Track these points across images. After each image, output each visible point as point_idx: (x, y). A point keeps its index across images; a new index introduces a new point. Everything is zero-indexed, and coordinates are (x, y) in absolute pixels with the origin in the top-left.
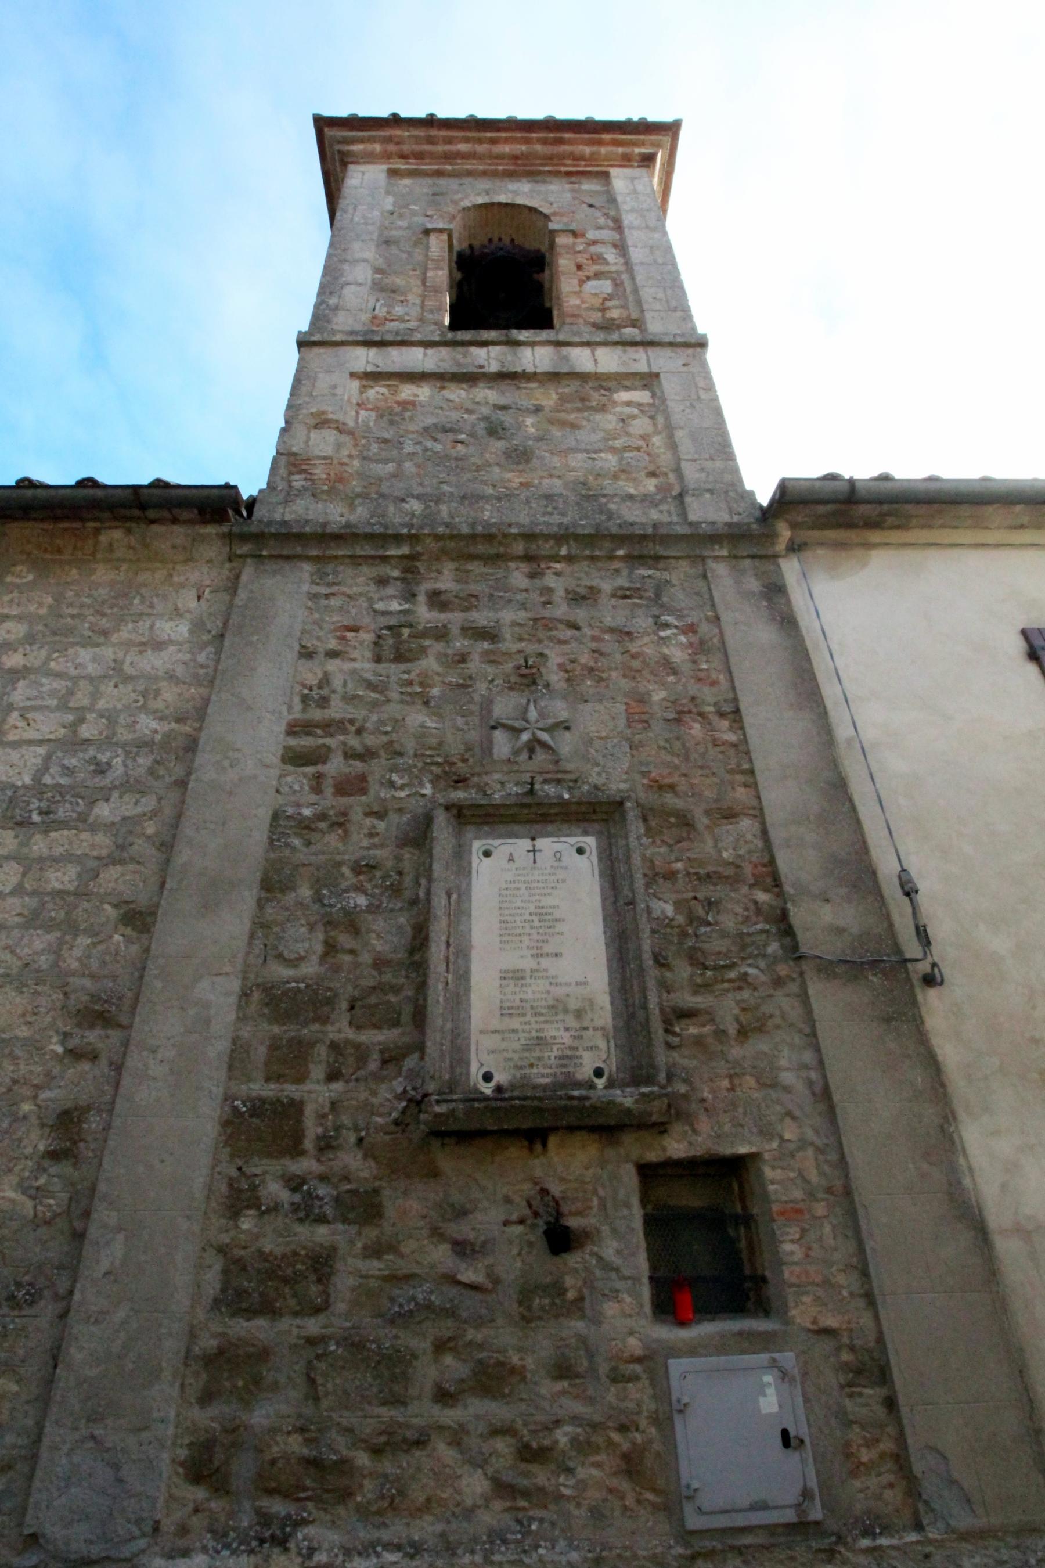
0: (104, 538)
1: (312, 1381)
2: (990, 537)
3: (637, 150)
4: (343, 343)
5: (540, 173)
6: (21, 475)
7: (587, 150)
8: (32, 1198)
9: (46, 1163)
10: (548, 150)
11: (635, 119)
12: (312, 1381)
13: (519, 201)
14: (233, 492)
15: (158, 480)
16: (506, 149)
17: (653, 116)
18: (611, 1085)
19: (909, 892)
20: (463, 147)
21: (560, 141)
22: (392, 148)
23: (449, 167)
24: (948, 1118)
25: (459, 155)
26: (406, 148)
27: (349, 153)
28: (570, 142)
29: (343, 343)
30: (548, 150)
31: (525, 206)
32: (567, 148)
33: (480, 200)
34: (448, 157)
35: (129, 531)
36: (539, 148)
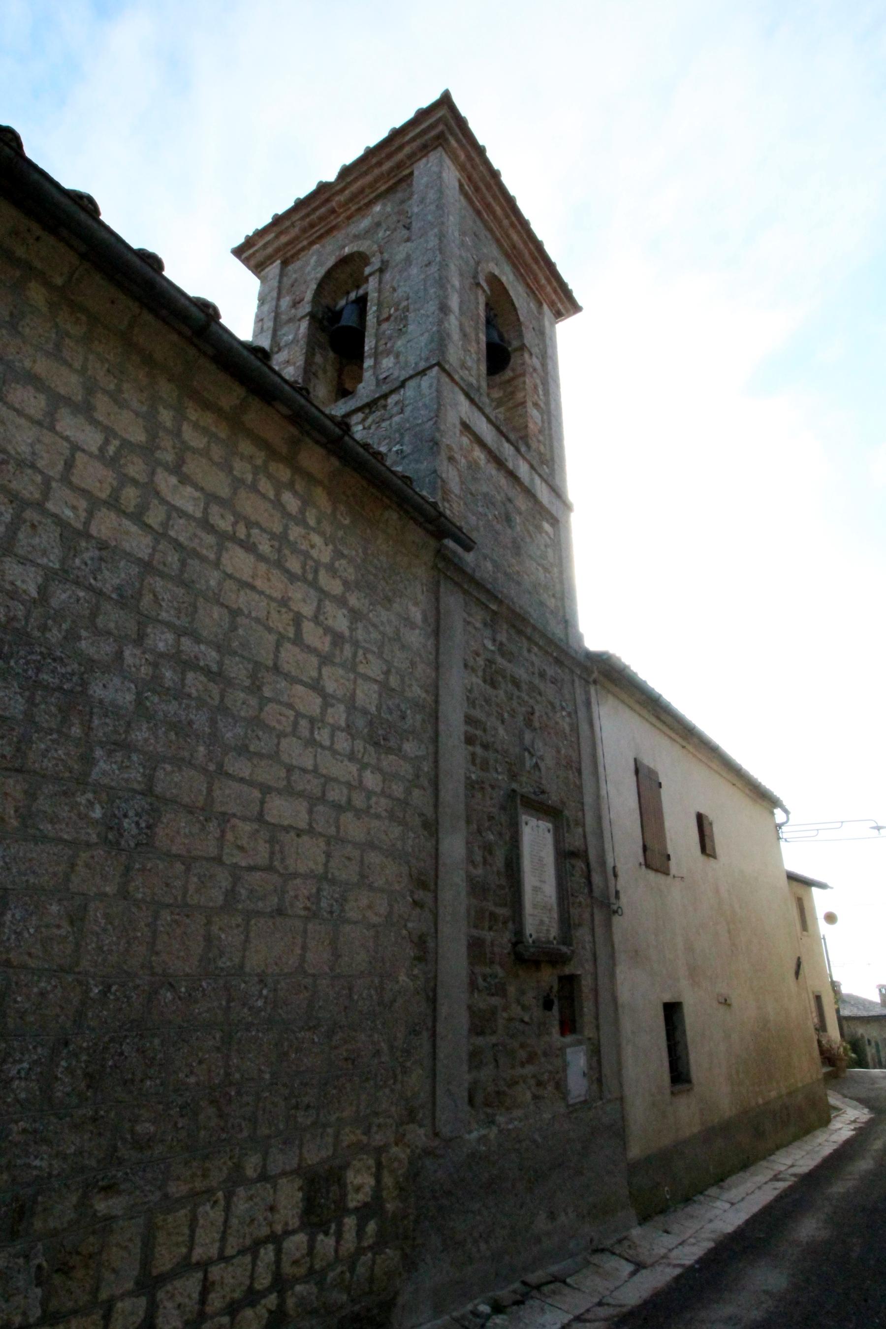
0: (386, 514)
1: (496, 1061)
2: (699, 756)
3: (559, 305)
4: (456, 383)
5: (518, 270)
6: (161, 255)
7: (543, 282)
8: (412, 980)
9: (416, 962)
10: (530, 260)
11: (570, 287)
12: (496, 1061)
13: (512, 293)
14: (472, 544)
15: (90, 200)
16: (515, 237)
17: (576, 295)
18: (558, 943)
19: (615, 875)
20: (498, 209)
21: (537, 262)
22: (468, 166)
23: (486, 216)
24: (614, 965)
25: (493, 213)
26: (475, 176)
27: (446, 140)
28: (540, 267)
29: (456, 383)
30: (530, 260)
31: (512, 300)
32: (535, 267)
33: (496, 273)
34: (488, 206)
35: (400, 519)
36: (527, 255)
